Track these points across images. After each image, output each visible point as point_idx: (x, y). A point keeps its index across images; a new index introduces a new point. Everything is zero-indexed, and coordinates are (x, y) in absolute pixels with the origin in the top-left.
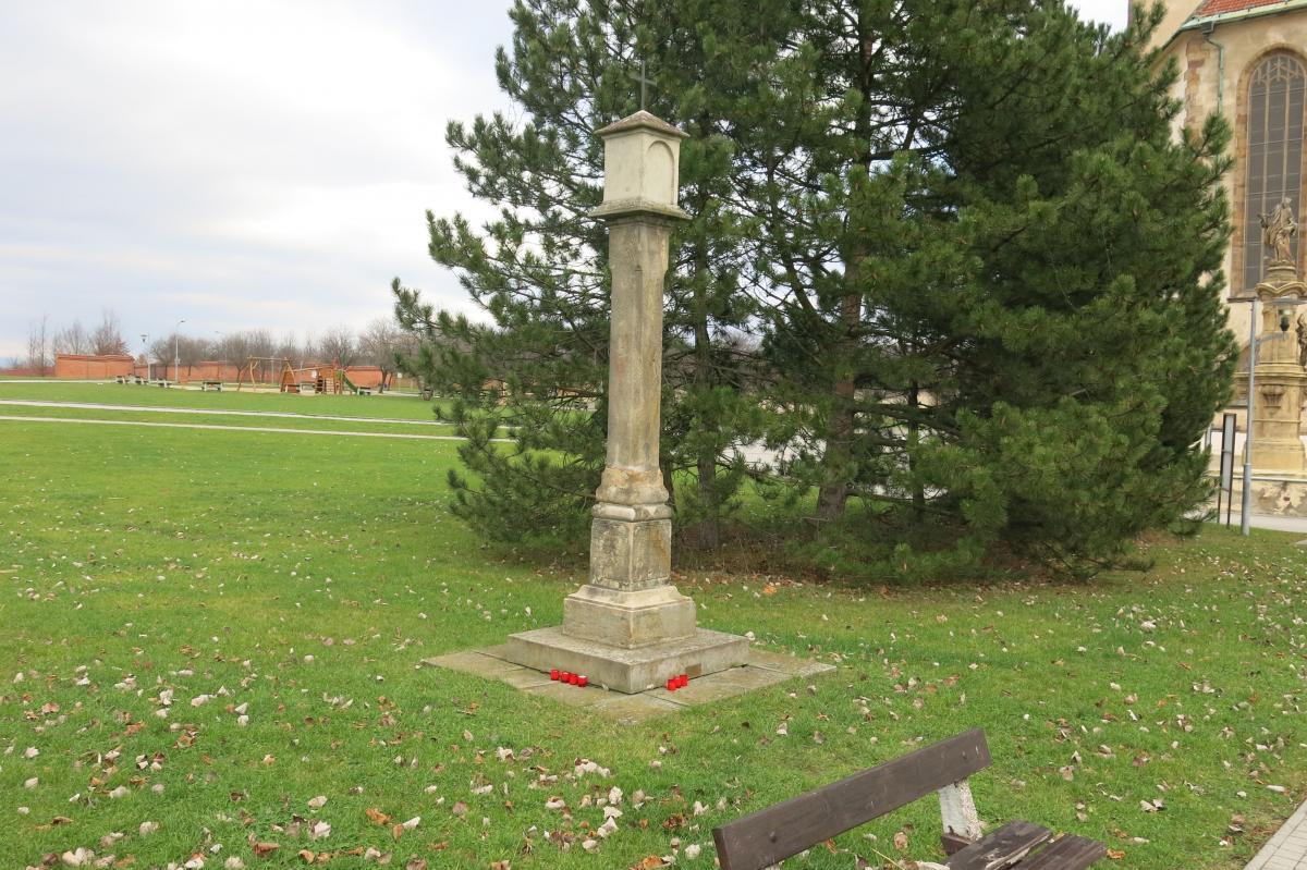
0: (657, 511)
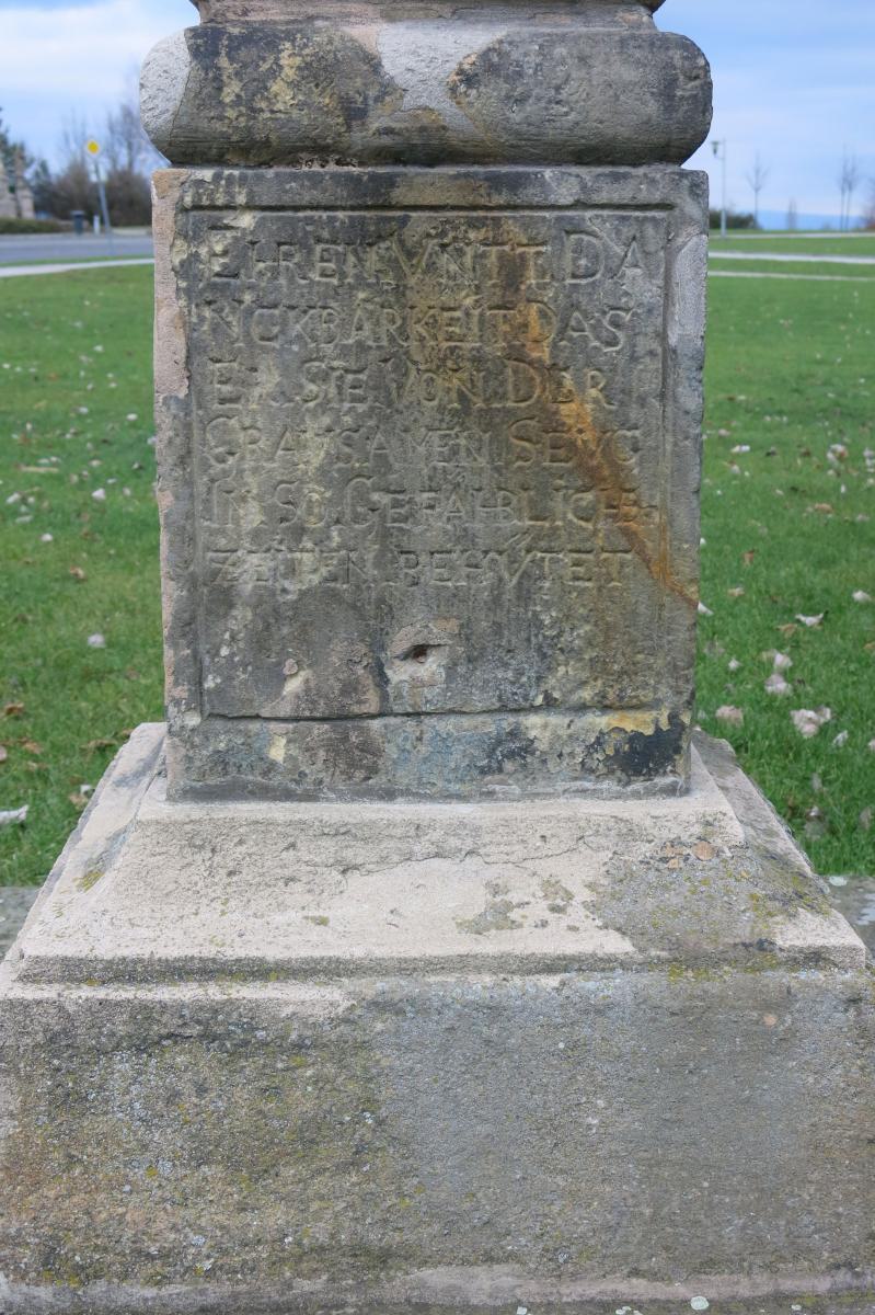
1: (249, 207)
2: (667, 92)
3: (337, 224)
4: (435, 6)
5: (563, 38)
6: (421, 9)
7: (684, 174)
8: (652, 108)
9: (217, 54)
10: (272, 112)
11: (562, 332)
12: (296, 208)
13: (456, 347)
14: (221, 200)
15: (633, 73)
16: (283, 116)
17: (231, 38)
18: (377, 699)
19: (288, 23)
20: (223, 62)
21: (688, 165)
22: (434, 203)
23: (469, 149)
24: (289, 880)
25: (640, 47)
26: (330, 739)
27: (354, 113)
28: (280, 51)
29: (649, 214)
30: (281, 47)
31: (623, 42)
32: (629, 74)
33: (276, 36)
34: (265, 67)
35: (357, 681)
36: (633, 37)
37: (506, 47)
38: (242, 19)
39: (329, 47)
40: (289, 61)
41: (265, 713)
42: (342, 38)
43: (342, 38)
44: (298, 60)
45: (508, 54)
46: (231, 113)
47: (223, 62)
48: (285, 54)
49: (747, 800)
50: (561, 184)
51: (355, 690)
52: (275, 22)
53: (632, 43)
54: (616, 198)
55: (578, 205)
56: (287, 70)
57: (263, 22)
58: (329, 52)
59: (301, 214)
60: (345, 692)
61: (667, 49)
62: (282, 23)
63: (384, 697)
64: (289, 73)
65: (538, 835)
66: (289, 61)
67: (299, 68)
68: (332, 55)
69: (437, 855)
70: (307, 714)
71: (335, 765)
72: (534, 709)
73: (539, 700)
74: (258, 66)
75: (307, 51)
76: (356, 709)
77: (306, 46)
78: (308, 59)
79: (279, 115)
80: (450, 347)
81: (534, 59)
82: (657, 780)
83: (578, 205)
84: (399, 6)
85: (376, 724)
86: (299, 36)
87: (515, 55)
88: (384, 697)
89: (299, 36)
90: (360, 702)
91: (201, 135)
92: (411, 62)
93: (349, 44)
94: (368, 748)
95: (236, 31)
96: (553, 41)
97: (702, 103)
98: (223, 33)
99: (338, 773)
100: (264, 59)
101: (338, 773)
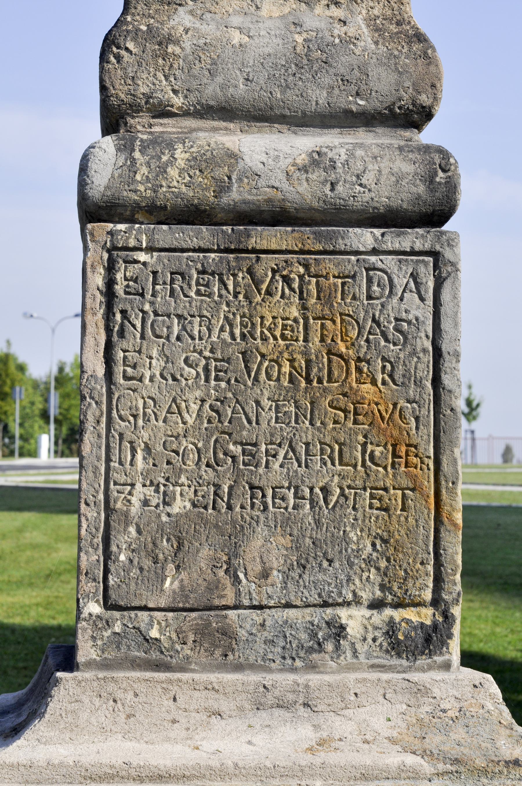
0: (317, 160)
1: (150, 249)
2: (430, 180)
3: (211, 261)
4: (276, 125)
5: (361, 145)
6: (267, 127)
7: (443, 233)
8: (421, 189)
9: (133, 150)
10: (169, 187)
11: (277, 412)
12: (183, 250)
13: (290, 344)
14: (132, 243)
15: (409, 167)
16: (176, 190)
17: (142, 140)
18: (233, 595)
19: (179, 133)
20: (137, 155)
21: (446, 227)
22: (442, 310)
23: (301, 215)
24: (174, 721)
25: (412, 151)
26: (197, 624)
27: (222, 188)
28: (176, 149)
29: (421, 258)
30: (176, 147)
31: (400, 149)
32: (408, 168)
33: (171, 140)
34: (165, 158)
35: (219, 581)
36: (407, 146)
37: (324, 150)
38: (148, 130)
39: (207, 148)
40: (181, 155)
41: (151, 605)
42: (216, 142)
43: (216, 142)
44: (187, 155)
45: (326, 154)
46: (141, 188)
47: (137, 155)
48: (179, 151)
49: (391, 232)
50: (365, 238)
51: (217, 587)
52: (170, 133)
53: (406, 149)
54: (397, 246)
55: (375, 252)
56: (179, 161)
57: (162, 132)
58: (208, 150)
59: (185, 254)
60: (209, 589)
61: (430, 153)
62: (174, 133)
63: (238, 594)
64: (181, 164)
65: (352, 692)
66: (181, 155)
67: (188, 160)
68: (210, 153)
69: (278, 706)
70: (181, 605)
71: (201, 645)
72: (347, 604)
73: (350, 597)
74: (160, 158)
75: (192, 150)
76: (217, 602)
77: (192, 147)
78: (194, 155)
79: (174, 189)
80: (286, 345)
81: (344, 157)
82: (435, 658)
83: (375, 252)
84: (253, 124)
85: (232, 614)
86: (187, 140)
87: (330, 155)
88: (238, 594)
89: (187, 140)
90: (223, 596)
91: (121, 202)
92: (264, 158)
93: (220, 146)
94: (227, 633)
95: (145, 137)
96: (357, 145)
97: (452, 188)
98: (137, 138)
99: (202, 650)
100: (163, 154)
101: (202, 650)
